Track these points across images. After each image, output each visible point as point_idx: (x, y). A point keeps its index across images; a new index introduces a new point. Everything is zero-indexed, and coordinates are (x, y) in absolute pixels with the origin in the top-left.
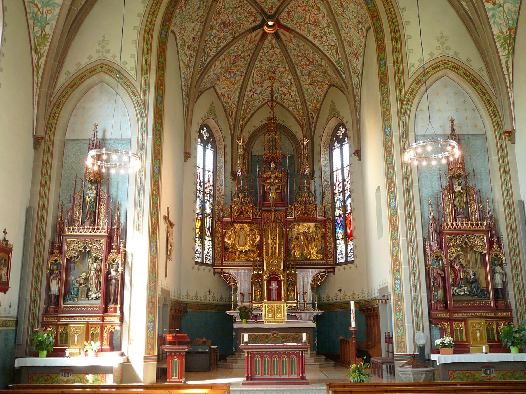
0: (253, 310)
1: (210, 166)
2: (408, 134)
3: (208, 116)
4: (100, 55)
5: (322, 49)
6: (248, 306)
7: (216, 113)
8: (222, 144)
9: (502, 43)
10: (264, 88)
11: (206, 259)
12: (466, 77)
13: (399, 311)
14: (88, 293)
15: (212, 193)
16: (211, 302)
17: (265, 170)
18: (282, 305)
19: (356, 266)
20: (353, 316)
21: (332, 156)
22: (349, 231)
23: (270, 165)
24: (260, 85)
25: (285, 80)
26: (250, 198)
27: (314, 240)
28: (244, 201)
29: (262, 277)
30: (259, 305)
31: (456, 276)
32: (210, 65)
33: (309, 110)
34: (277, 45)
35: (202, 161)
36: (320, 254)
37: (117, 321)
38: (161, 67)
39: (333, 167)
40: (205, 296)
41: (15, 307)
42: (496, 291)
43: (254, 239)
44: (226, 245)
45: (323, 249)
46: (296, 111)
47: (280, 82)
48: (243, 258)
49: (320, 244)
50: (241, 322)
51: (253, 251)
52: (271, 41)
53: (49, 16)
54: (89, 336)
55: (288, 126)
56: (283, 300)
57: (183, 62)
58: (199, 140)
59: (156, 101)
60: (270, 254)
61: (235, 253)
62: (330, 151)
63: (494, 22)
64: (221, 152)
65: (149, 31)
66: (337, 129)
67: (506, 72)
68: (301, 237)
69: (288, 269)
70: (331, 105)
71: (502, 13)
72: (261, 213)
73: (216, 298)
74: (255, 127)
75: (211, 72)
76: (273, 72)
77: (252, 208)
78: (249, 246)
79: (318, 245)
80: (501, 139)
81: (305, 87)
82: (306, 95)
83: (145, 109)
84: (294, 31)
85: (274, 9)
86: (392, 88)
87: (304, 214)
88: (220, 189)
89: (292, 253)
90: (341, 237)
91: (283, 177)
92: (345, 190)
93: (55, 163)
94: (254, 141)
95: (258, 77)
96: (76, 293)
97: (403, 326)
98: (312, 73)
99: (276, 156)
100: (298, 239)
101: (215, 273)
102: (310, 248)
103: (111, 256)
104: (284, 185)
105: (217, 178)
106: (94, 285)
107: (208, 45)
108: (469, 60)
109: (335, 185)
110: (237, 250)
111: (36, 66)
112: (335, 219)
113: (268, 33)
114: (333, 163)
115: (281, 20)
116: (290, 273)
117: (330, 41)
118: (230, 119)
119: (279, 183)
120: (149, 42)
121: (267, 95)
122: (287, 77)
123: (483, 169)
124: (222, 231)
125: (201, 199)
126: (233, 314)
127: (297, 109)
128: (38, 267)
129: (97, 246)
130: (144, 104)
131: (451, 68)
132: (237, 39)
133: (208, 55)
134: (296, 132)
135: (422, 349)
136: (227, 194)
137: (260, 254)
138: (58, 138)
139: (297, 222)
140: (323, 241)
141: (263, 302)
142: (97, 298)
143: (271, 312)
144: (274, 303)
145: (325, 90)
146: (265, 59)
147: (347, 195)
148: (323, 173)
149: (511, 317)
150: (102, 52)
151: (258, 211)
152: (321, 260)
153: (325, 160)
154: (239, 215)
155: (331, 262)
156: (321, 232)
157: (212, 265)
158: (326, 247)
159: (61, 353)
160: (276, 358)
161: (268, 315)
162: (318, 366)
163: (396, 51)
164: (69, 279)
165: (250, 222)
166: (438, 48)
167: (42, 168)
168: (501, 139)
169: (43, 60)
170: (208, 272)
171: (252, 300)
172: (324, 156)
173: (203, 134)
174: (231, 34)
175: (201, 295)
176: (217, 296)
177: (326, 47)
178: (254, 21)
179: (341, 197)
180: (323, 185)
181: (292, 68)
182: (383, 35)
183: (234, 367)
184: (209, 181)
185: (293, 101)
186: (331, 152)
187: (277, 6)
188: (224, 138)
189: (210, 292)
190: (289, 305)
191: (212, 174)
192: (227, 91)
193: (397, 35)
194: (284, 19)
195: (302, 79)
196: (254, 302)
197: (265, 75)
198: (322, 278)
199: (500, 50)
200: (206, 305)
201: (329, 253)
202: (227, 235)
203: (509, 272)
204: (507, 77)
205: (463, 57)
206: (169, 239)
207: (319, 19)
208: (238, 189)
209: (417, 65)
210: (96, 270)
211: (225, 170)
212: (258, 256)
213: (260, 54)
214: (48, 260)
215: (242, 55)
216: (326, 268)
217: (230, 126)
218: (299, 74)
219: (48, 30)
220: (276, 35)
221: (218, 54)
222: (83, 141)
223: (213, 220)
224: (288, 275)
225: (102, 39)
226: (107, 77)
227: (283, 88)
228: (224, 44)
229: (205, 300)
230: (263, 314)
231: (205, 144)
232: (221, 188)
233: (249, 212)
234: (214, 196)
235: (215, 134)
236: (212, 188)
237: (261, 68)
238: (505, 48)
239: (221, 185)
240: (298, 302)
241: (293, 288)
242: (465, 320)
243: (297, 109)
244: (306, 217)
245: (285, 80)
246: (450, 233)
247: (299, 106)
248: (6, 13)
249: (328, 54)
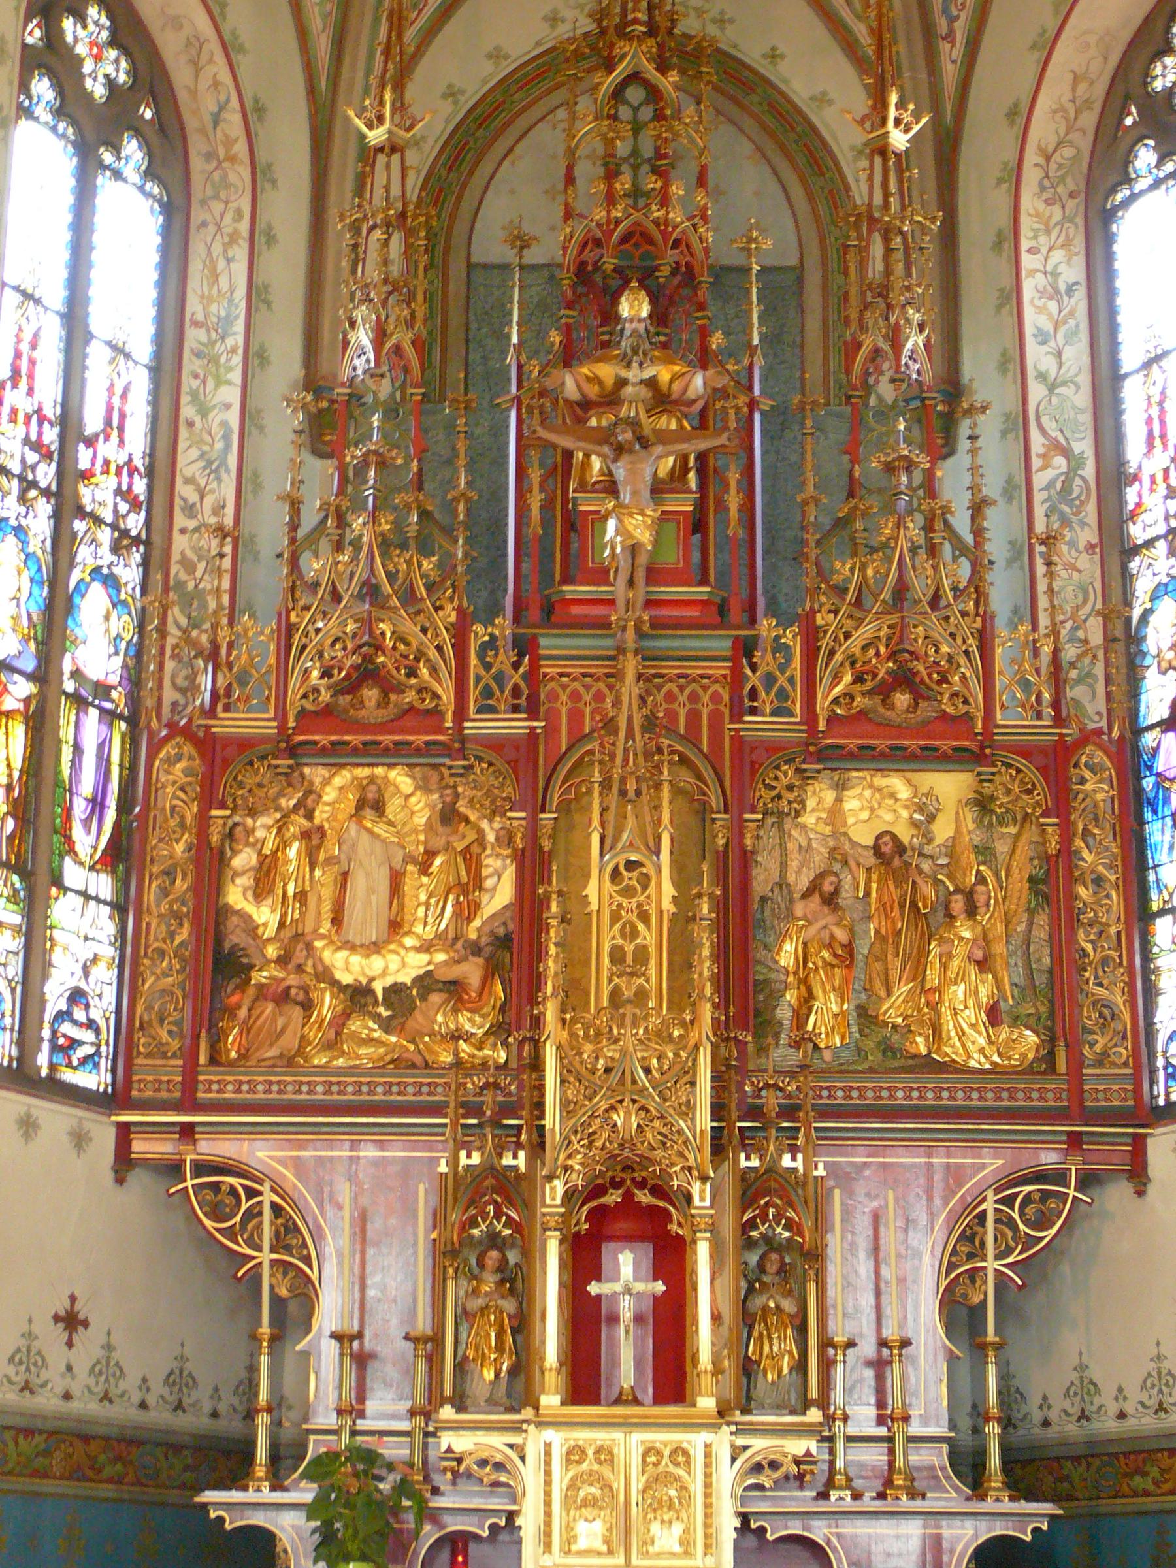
0: (443, 1481)
6: (395, 1450)
8: (232, 159)
11: (55, 1048)
15: (135, 523)
16: (75, 1406)
18: (696, 1441)
21: (1109, 257)
27: (971, 911)
28: (391, 577)
29: (528, 1205)
30: (497, 1441)
35: (65, 256)
36: (1015, 1021)
39: (1114, 345)
44: (235, 937)
45: (1041, 980)
48: (370, 1041)
49: (1017, 941)
51: (454, 989)
55: (752, 53)
56: (707, 1403)
61: (307, 1006)
62: (1096, 224)
68: (851, 885)
69: (746, 1141)
73: (130, 1383)
74: (496, 55)
78: (426, 947)
79: (999, 948)
87: (884, 691)
88: (209, 501)
89: (784, 1014)
91: (721, 393)
94: (486, 167)
99: (663, 224)
100: (831, 901)
101: (124, 1162)
102: (933, 976)
105: (188, 411)
109: (1136, 478)
110: (325, 975)
112: (1137, 752)
114: (1112, 312)
116: (771, 1170)
119: (680, 436)
124: (203, 819)
125: (34, 546)
126: (258, 1519)
137: (511, 1015)
140: (1042, 919)
141: (528, 1413)
143: (591, 1503)
144: (626, 1424)
148: (1036, 391)
151: (504, 659)
152: (1028, 1071)
154: (351, 687)
161: (569, 1527)
171: (435, 1398)
173: (81, 49)
180: (1040, 479)
184: (115, 424)
186: (1097, 234)
189: (71, 1321)
190: (759, 1444)
191: (141, 383)
196: (447, 1412)
198: (1042, 1223)
200: (29, 1432)
201: (1089, 1017)
202: (244, 859)
216: (1074, 1142)
223: (132, 740)
229: (27, 1387)
230: (529, 1523)
233: (434, 670)
235: (181, 75)
236: (140, 486)
239: (213, 468)
240: (830, 1419)
241: (789, 1306)
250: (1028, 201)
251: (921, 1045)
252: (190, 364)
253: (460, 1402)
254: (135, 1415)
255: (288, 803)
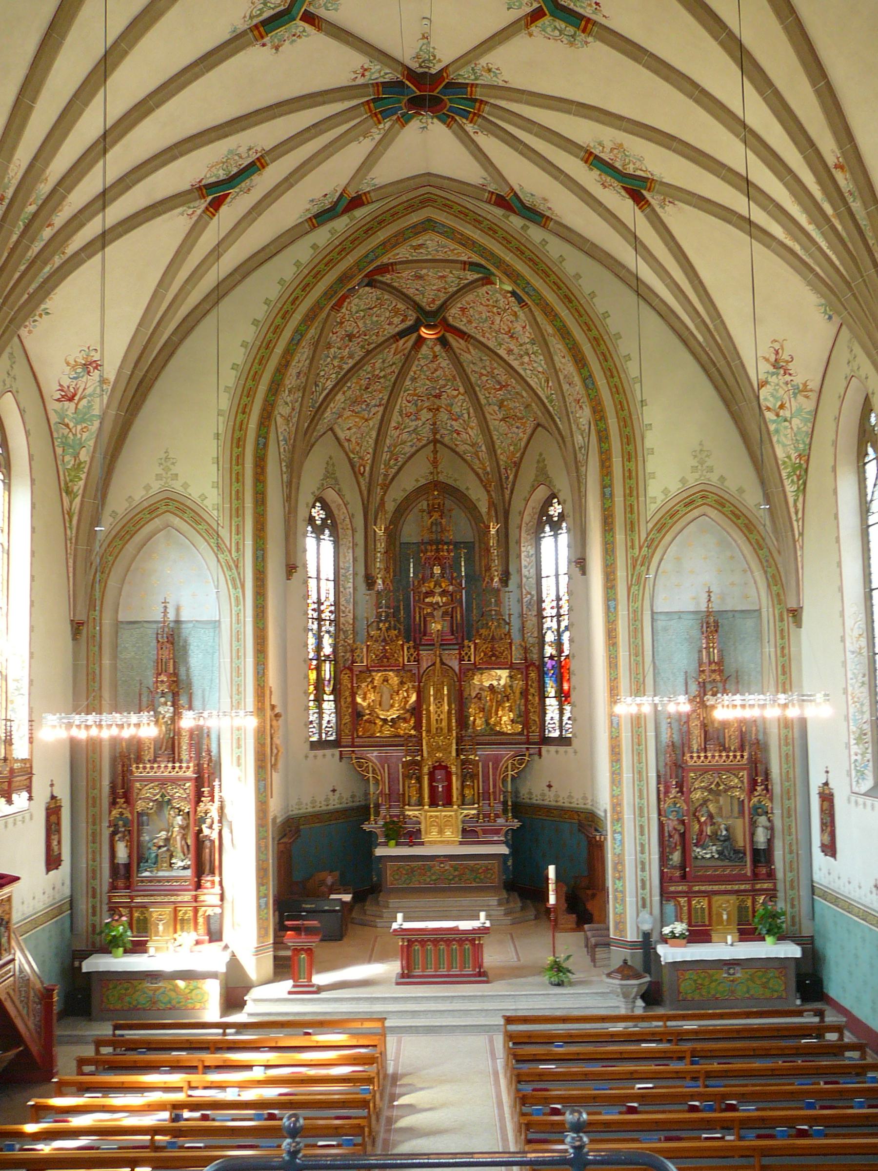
1: (328, 571)
2: (642, 614)
3: (323, 485)
4: (162, 483)
5: (522, 372)
7: (337, 474)
9: (789, 473)
10: (420, 423)
12: (735, 519)
13: (619, 879)
14: (171, 859)
17: (423, 577)
19: (575, 752)
20: (552, 887)
22: (566, 687)
23: (432, 569)
24: (413, 417)
25: (458, 410)
26: (399, 629)
29: (420, 770)
30: (416, 812)
31: (701, 831)
32: (325, 404)
33: (501, 463)
34: (444, 354)
36: (517, 723)
37: (216, 900)
38: (260, 499)
40: (327, 800)
41: (68, 882)
42: (756, 852)
43: (406, 699)
44: (360, 709)
46: (478, 462)
47: (450, 412)
50: (386, 844)
52: (432, 348)
53: (85, 435)
54: (177, 923)
55: (462, 488)
57: (282, 416)
58: (309, 528)
59: (256, 558)
60: (434, 731)
63: (778, 441)
64: (346, 542)
65: (239, 442)
66: (548, 503)
67: (794, 517)
68: (484, 694)
70: (538, 462)
71: (789, 431)
72: (418, 655)
73: (344, 800)
75: (328, 414)
76: (435, 396)
77: (402, 645)
80: (782, 620)
81: (493, 424)
82: (495, 437)
83: (239, 574)
84: (472, 337)
85: (438, 303)
86: (620, 537)
87: (490, 657)
89: (470, 722)
90: (553, 694)
92: (561, 616)
93: (106, 662)
95: (409, 405)
96: (154, 860)
97: (623, 901)
98: (505, 403)
100: (480, 699)
101: (341, 758)
102: (500, 713)
103: (202, 807)
104: (456, 607)
105: (342, 589)
106: (179, 849)
107: (322, 373)
108: (741, 490)
111: (68, 513)
113: (425, 339)
115: (450, 319)
117: (535, 365)
118: (361, 480)
120: (239, 460)
121: (426, 433)
122: (461, 404)
123: (752, 666)
127: (479, 459)
128: (95, 821)
129: (179, 793)
130: (237, 567)
131: (713, 503)
132: (373, 354)
133: (323, 387)
134: (478, 500)
135: (647, 935)
136: (359, 618)
138: (107, 622)
139: (476, 668)
142: (184, 868)
145: (529, 431)
146: (423, 377)
147: (563, 624)
148: (524, 580)
149: (775, 889)
150: (167, 478)
151: (412, 651)
153: (528, 556)
155: (535, 736)
156: (519, 684)
157: (336, 744)
158: (527, 711)
159: (139, 947)
160: (442, 946)
162: (509, 922)
163: (629, 475)
164: (142, 838)
165: (401, 670)
166: (694, 469)
167: (88, 670)
168: (782, 620)
169: (78, 500)
170: (330, 757)
172: (527, 549)
174: (363, 347)
175: (321, 799)
176: (346, 795)
177: (529, 372)
178: (403, 321)
179: (554, 625)
180: (525, 600)
181: (471, 391)
182: (610, 446)
183: (379, 925)
185: (473, 445)
187: (442, 300)
188: (352, 517)
189: (334, 791)
190: (466, 812)
192: (355, 433)
193: (631, 448)
194: (454, 317)
195: (488, 409)
197: (422, 401)
199: (787, 483)
203: (778, 823)
204: (795, 524)
205: (732, 485)
206: (274, 739)
207: (517, 330)
208: (379, 615)
209: (661, 497)
210: (181, 827)
211: (355, 574)
212: (414, 728)
213: (414, 368)
214: (110, 812)
215: (382, 374)
217: (361, 492)
218: (483, 401)
219: (84, 456)
220: (443, 342)
221: (340, 383)
222: (145, 625)
224: (464, 762)
225: (164, 455)
226: (177, 521)
227: (454, 423)
228: (350, 365)
231: (318, 531)
232: (347, 607)
234: (336, 622)
235: (336, 512)
237: (415, 390)
238: (792, 481)
239: (348, 602)
242: (709, 894)
243: (479, 459)
244: (493, 661)
245: (458, 410)
246: (695, 769)
247: (483, 455)
248: (33, 463)
249: (532, 383)
250: (523, 534)
251: (498, 729)
252: (342, 578)
253: (409, 805)
254: (346, 805)
255: (369, 680)
